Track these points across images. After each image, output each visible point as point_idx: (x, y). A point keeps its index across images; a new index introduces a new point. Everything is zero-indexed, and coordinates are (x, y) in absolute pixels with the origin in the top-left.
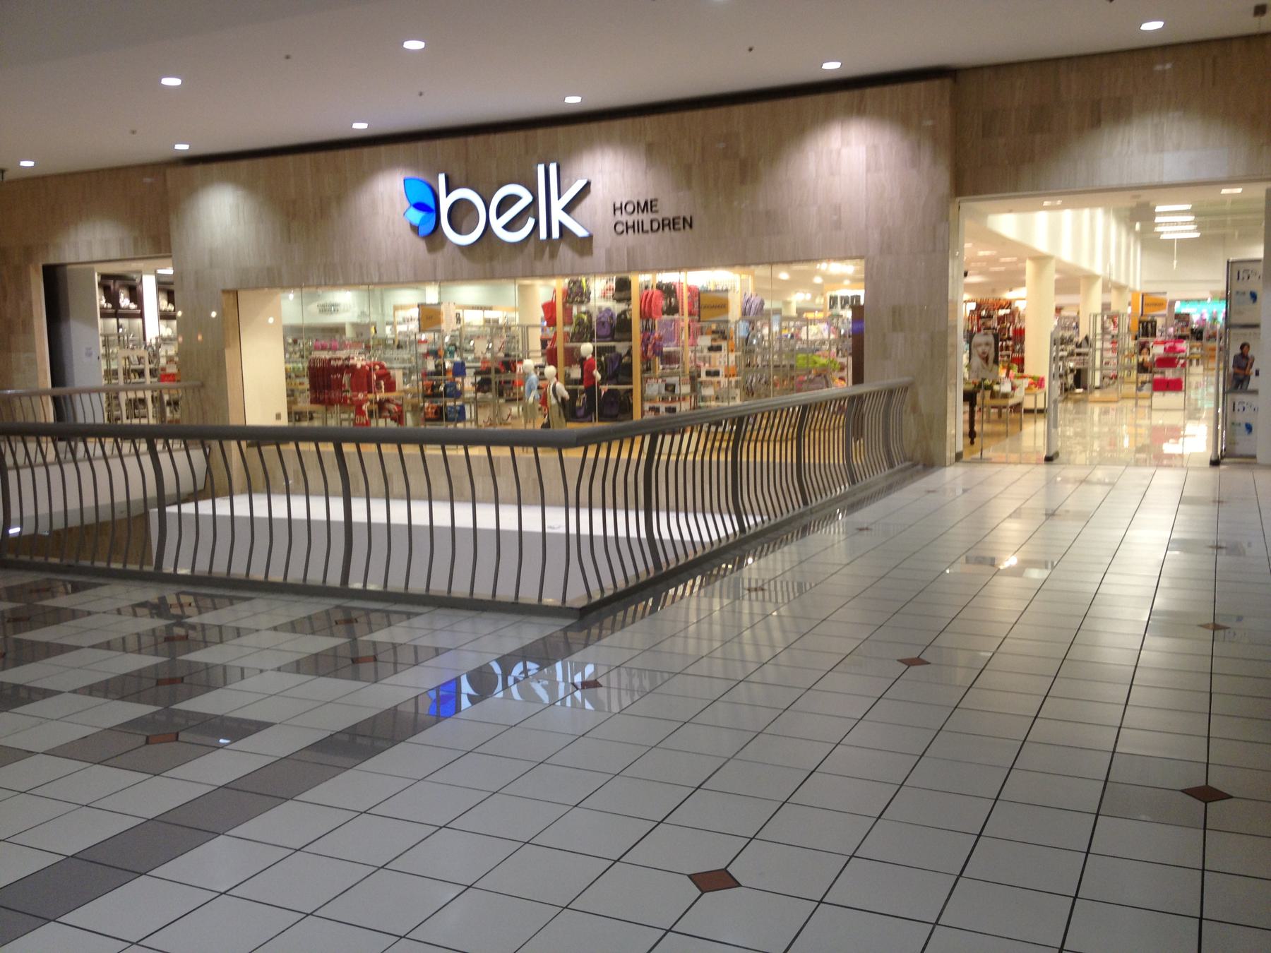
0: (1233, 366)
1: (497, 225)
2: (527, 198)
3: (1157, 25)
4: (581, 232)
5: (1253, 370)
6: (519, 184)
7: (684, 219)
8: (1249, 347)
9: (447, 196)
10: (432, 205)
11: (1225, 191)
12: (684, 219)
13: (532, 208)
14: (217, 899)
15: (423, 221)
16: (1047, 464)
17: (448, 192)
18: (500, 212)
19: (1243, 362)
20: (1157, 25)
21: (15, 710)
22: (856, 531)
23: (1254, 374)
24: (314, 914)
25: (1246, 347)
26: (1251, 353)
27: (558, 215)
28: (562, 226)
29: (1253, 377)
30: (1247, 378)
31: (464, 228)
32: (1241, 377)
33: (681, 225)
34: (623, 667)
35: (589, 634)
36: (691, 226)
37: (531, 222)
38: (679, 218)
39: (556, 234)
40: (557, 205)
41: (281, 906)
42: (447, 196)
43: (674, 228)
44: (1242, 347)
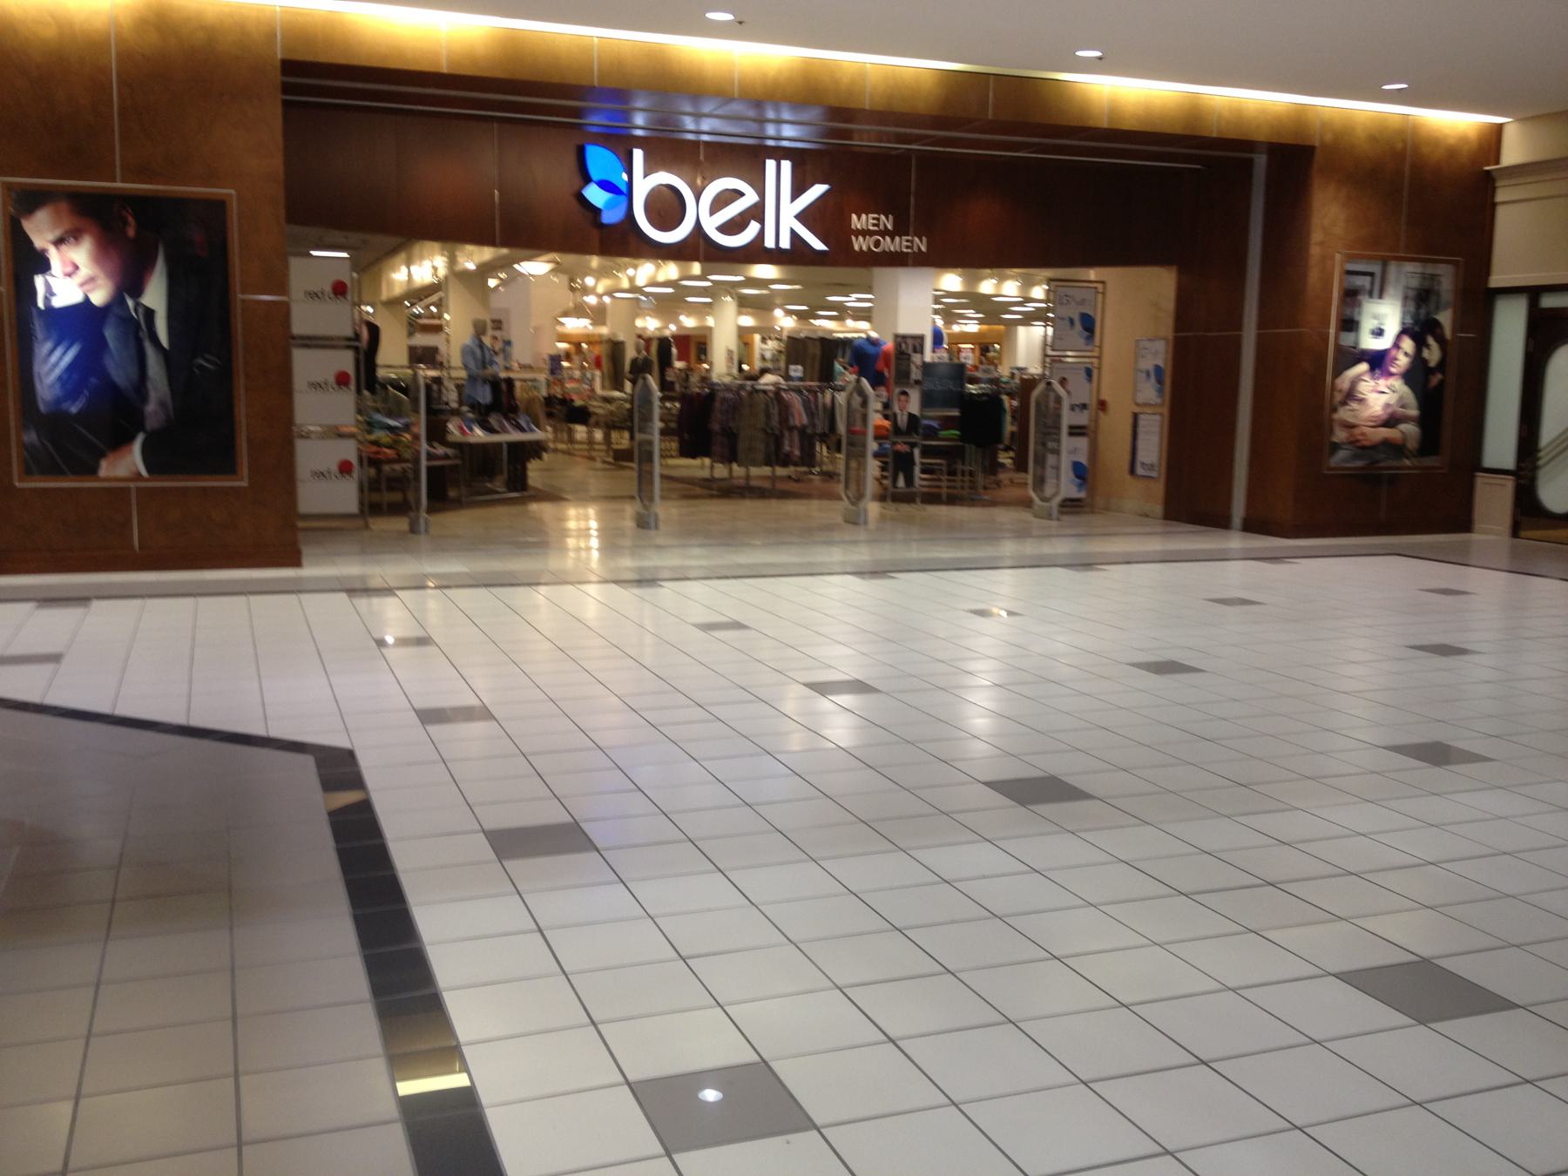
1: (711, 225)
2: (751, 197)
10: (624, 188)
13: (757, 212)
18: (716, 206)
28: (794, 234)
39: (785, 243)
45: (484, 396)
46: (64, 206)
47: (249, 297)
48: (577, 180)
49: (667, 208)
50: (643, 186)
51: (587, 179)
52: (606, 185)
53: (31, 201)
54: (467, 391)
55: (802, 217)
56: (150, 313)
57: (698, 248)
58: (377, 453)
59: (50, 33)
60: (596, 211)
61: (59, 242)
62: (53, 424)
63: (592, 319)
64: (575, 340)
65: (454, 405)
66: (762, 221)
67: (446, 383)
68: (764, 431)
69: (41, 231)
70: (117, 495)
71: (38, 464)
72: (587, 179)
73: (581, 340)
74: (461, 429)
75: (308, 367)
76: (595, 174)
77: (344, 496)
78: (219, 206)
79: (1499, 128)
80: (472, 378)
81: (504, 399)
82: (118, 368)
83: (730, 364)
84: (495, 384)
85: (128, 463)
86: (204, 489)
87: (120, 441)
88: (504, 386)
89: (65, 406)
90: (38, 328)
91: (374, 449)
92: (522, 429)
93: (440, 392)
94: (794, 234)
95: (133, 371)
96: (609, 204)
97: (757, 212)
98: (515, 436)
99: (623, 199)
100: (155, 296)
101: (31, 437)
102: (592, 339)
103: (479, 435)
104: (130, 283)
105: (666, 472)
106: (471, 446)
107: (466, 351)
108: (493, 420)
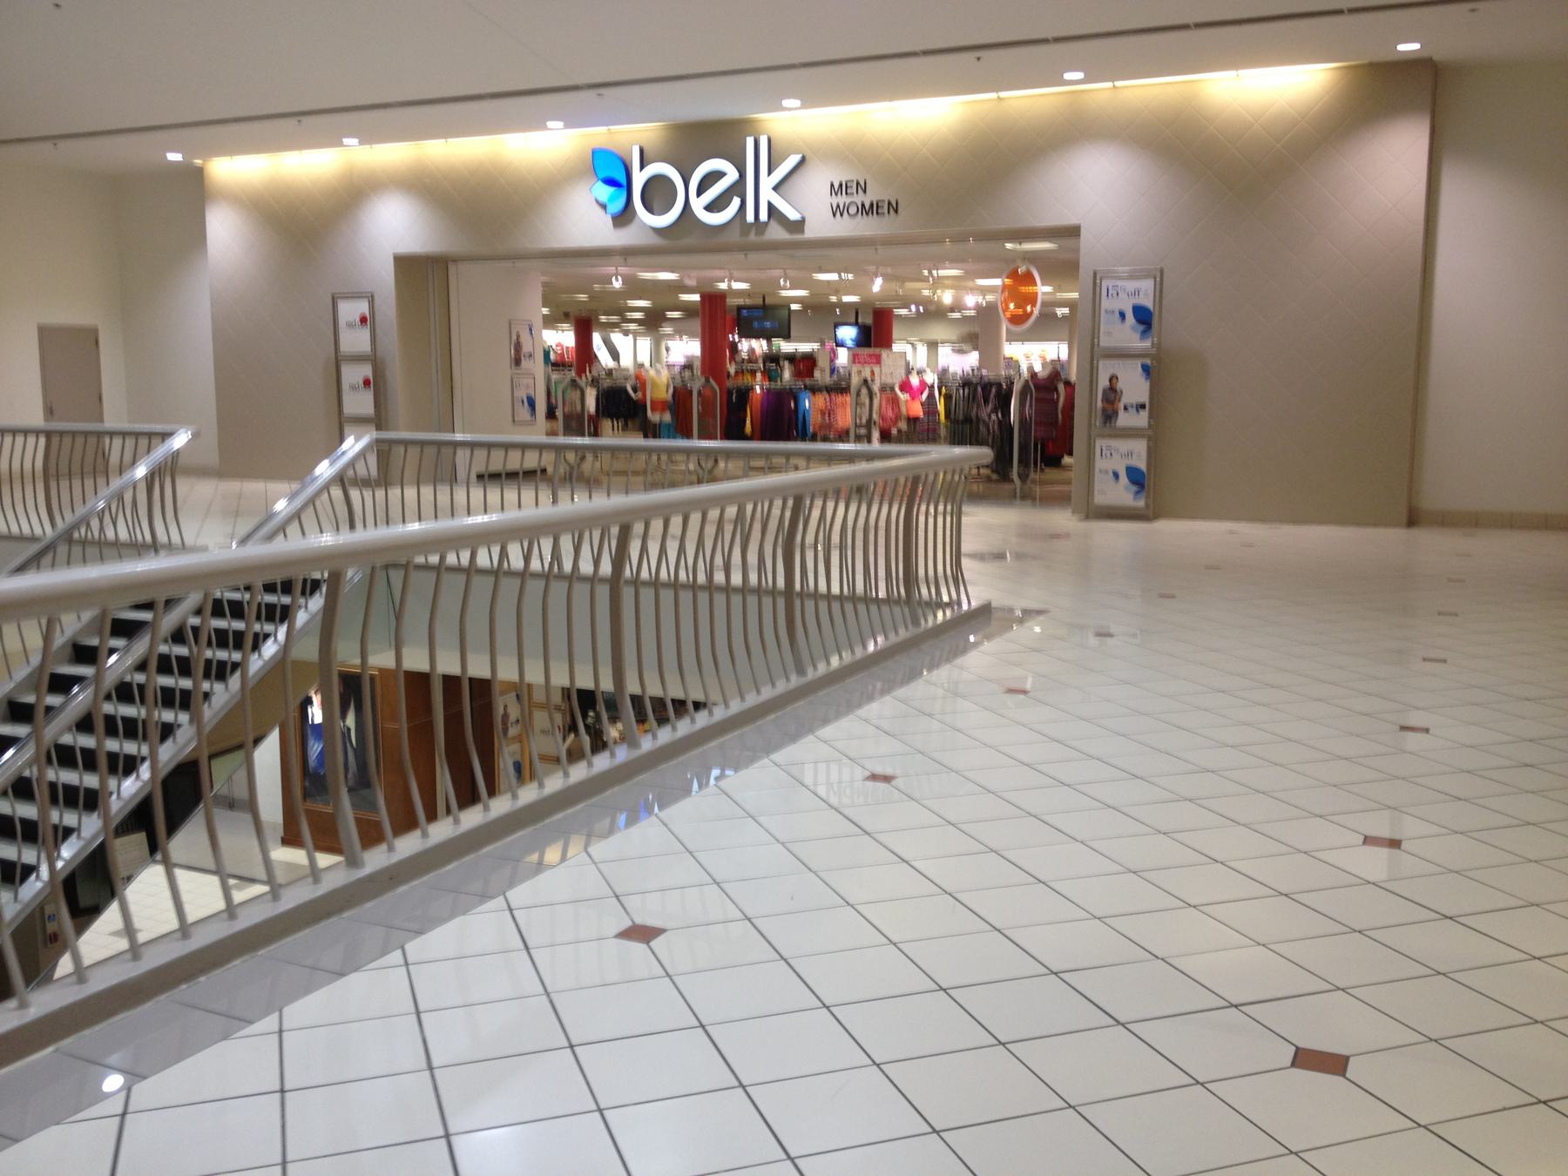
0: (1102, 401)
1: (698, 205)
2: (732, 175)
3: (1415, 46)
4: (793, 215)
5: (1121, 406)
6: (728, 160)
7: (889, 203)
8: (1117, 378)
9: (641, 170)
10: (623, 181)
11: (1009, 246)
12: (889, 203)
13: (738, 188)
14: (1133, 1019)
15: (612, 199)
16: (1024, 502)
17: (642, 167)
18: (701, 191)
19: (1112, 396)
20: (1415, 46)
21: (473, 911)
22: (159, 857)
23: (1122, 408)
24: (1229, 1005)
25: (1114, 381)
26: (1120, 385)
27: (767, 195)
28: (770, 206)
29: (1121, 413)
30: (1116, 413)
31: (656, 207)
32: (1110, 412)
33: (886, 211)
34: (120, 1090)
35: (613, 822)
36: (896, 211)
37: (736, 202)
38: (883, 201)
39: (764, 216)
40: (767, 182)
41: (1059, 1093)
42: (641, 170)
43: (877, 213)
44: (1111, 380)
94: (770, 206)
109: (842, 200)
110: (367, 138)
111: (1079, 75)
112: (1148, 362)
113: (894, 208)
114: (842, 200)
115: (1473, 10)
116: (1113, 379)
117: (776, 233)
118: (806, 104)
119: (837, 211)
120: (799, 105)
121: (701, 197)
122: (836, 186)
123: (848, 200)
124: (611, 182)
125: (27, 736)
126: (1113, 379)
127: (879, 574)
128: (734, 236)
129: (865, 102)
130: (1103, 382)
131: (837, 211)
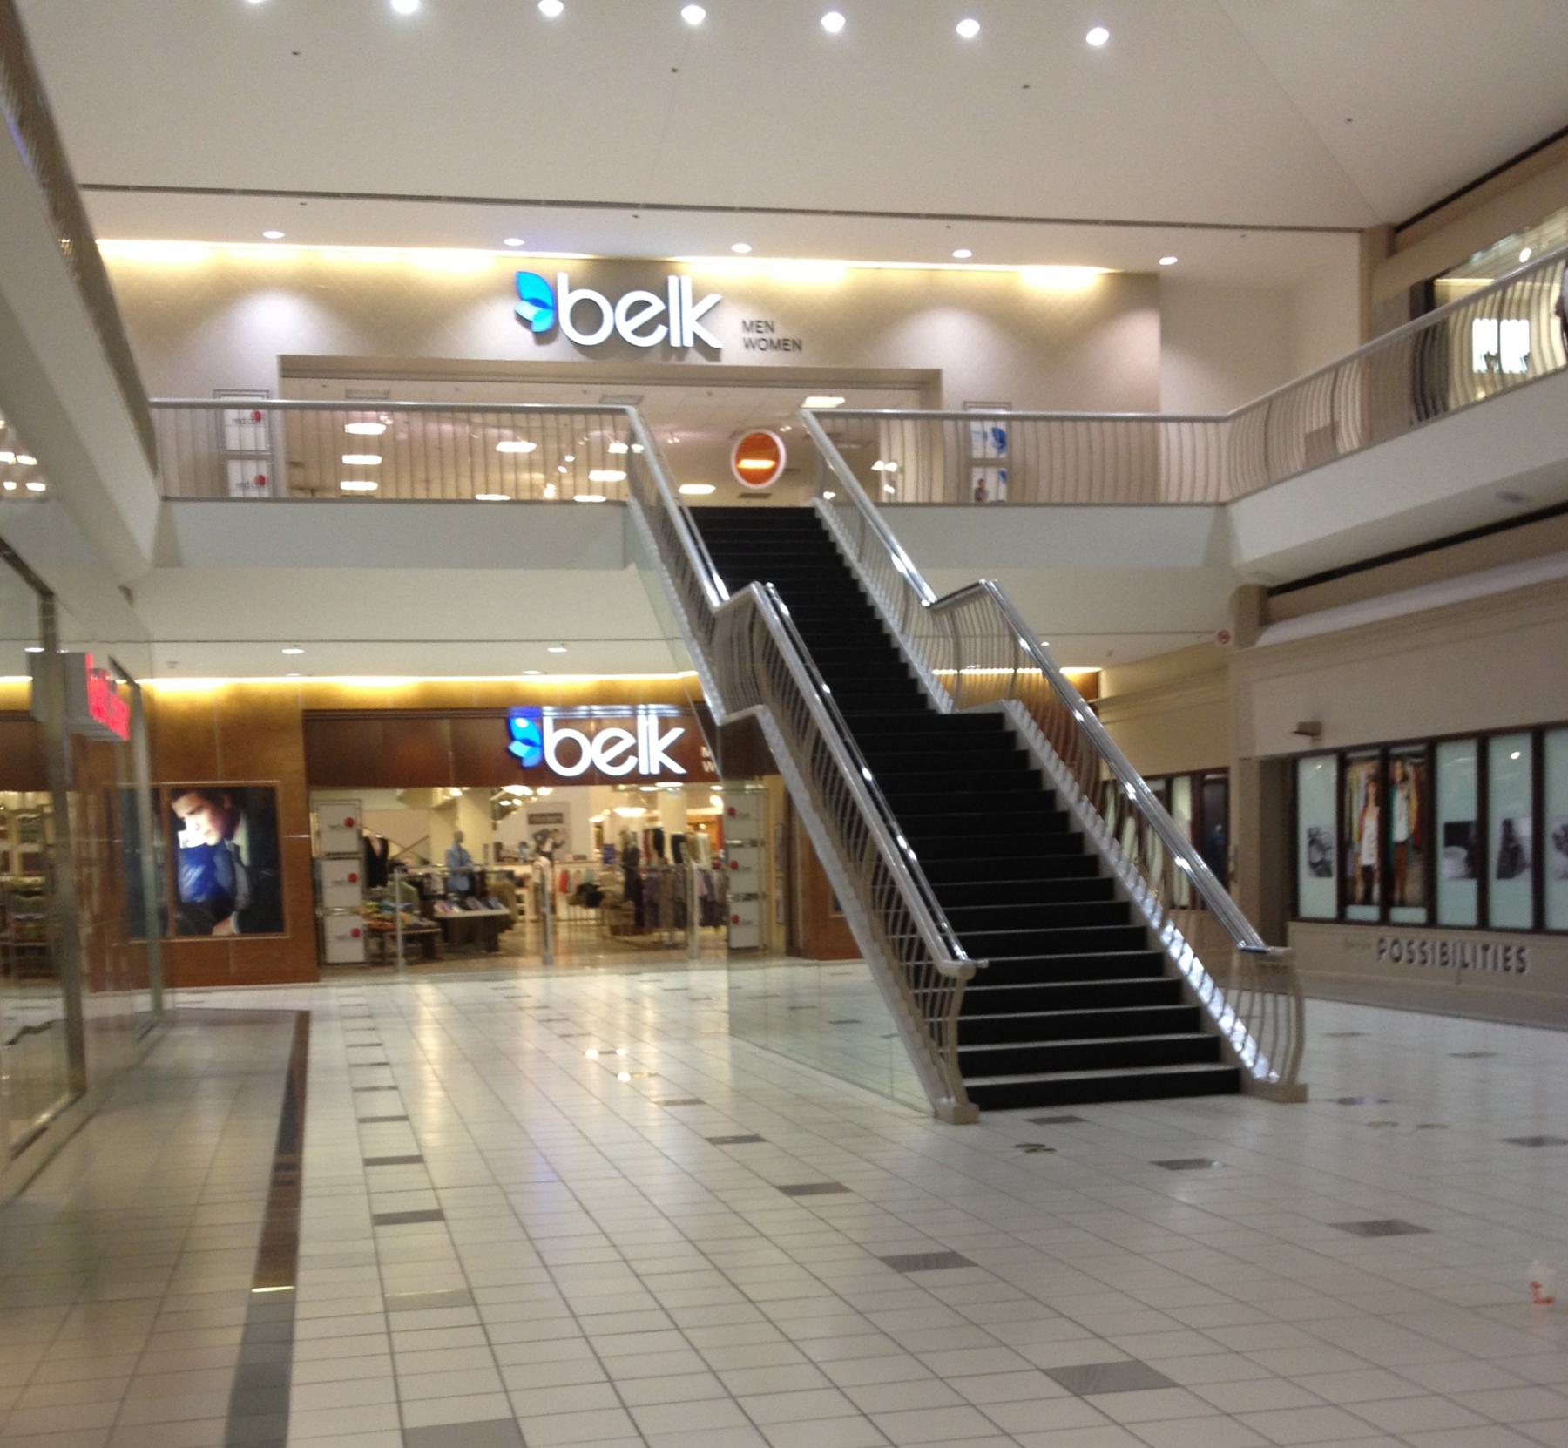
1: (626, 330)
2: (657, 306)
4: (713, 343)
13: (663, 318)
39: (689, 342)
40: (691, 313)
45: (463, 885)
46: (193, 795)
47: (287, 837)
48: (506, 738)
49: (569, 752)
50: (552, 738)
51: (512, 738)
52: (527, 742)
53: (178, 793)
54: (450, 882)
55: (668, 751)
56: (237, 848)
57: (593, 777)
58: (381, 925)
59: (184, 707)
60: (520, 759)
61: (192, 813)
62: (188, 908)
63: (646, 807)
64: (694, 821)
65: (441, 892)
66: (667, 324)
67: (434, 877)
68: (672, 900)
69: (182, 808)
70: (223, 945)
71: (184, 930)
72: (512, 738)
73: (698, 821)
74: (443, 908)
75: (332, 872)
76: (517, 734)
77: (355, 951)
78: (270, 792)
79: (1096, 675)
80: (454, 873)
81: (478, 885)
82: (222, 878)
83: (521, 861)
84: (471, 876)
85: (229, 928)
86: (268, 940)
87: (221, 916)
88: (478, 878)
89: (195, 898)
90: (182, 858)
91: (380, 923)
92: (491, 907)
93: (429, 883)
94: (696, 337)
95: (230, 878)
96: (529, 754)
97: (663, 318)
98: (484, 912)
99: (537, 750)
100: (240, 839)
101: (178, 916)
102: (709, 820)
103: (456, 912)
104: (228, 833)
105: (939, 998)
106: (453, 920)
107: (450, 855)
108: (470, 901)
109: (754, 336)
110: (764, 247)
111: (519, 242)
112: (1003, 469)
113: (798, 346)
114: (754, 336)
115: (302, 204)
116: (981, 482)
117: (696, 359)
118: (289, 239)
119: (749, 344)
120: (282, 238)
121: (630, 321)
122: (748, 323)
123: (759, 336)
124: (536, 302)
125: (353, 858)
126: (981, 482)
127: (802, 649)
128: (656, 359)
129: (1025, 263)
130: (975, 485)
131: (749, 344)
